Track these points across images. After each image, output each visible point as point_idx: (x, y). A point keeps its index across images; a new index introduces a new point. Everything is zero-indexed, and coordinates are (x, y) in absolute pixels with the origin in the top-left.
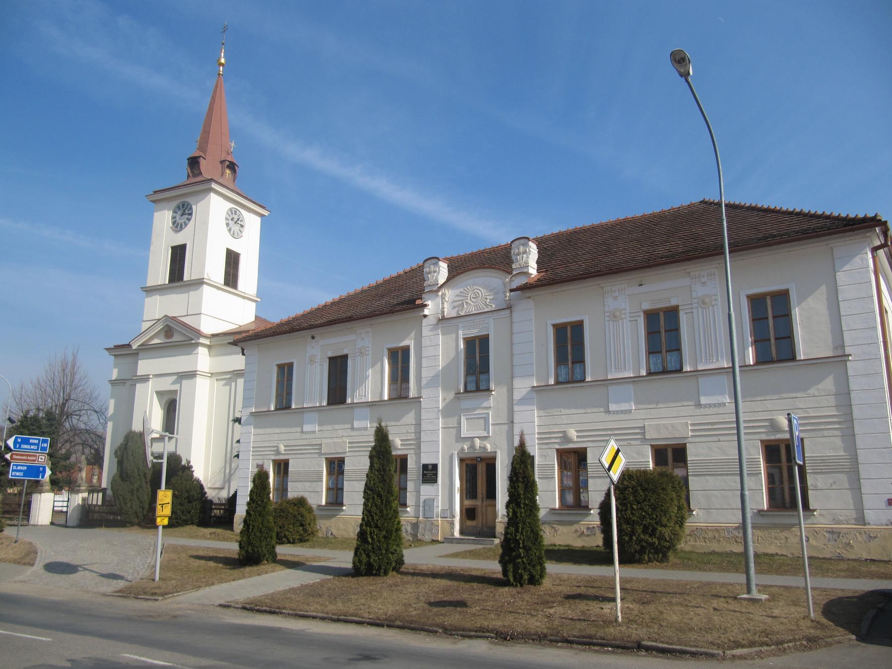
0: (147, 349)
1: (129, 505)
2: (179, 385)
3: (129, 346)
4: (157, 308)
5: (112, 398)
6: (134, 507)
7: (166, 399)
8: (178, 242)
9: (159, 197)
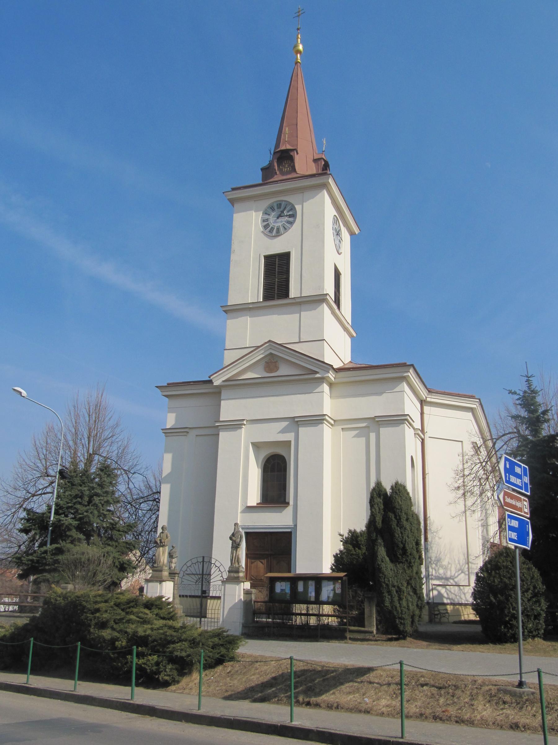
0: (236, 385)
1: (404, 603)
2: (293, 434)
3: (210, 382)
4: (247, 334)
5: (167, 451)
6: (411, 607)
7: (265, 453)
8: (277, 247)
9: (238, 196)
